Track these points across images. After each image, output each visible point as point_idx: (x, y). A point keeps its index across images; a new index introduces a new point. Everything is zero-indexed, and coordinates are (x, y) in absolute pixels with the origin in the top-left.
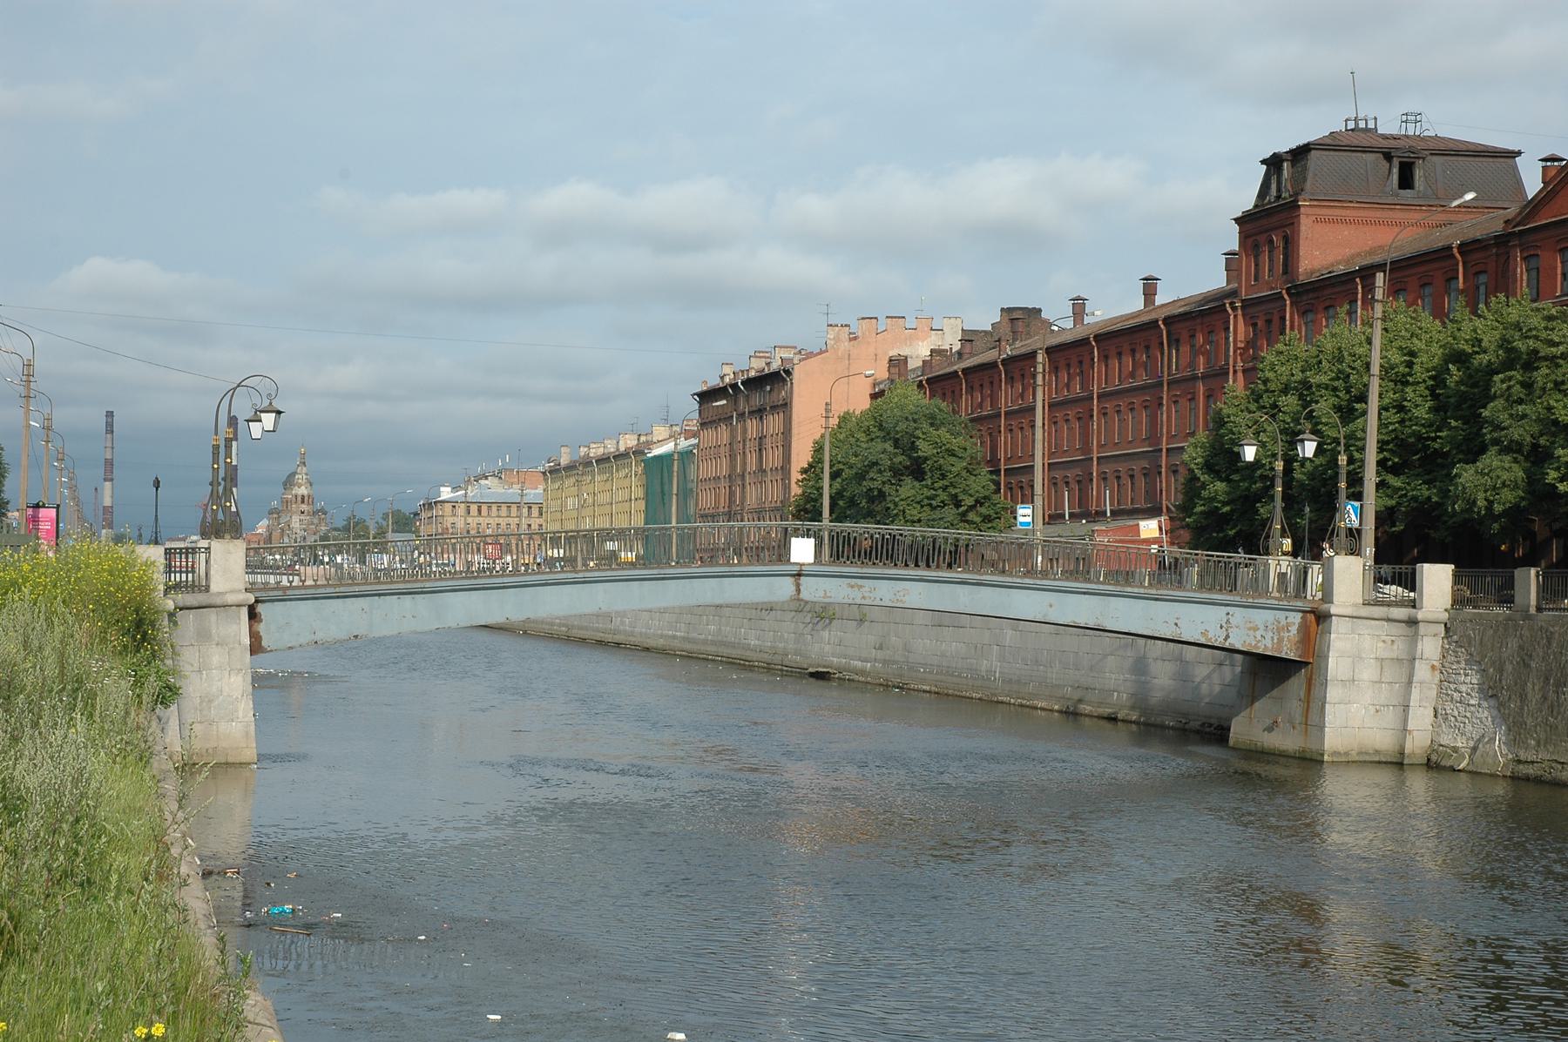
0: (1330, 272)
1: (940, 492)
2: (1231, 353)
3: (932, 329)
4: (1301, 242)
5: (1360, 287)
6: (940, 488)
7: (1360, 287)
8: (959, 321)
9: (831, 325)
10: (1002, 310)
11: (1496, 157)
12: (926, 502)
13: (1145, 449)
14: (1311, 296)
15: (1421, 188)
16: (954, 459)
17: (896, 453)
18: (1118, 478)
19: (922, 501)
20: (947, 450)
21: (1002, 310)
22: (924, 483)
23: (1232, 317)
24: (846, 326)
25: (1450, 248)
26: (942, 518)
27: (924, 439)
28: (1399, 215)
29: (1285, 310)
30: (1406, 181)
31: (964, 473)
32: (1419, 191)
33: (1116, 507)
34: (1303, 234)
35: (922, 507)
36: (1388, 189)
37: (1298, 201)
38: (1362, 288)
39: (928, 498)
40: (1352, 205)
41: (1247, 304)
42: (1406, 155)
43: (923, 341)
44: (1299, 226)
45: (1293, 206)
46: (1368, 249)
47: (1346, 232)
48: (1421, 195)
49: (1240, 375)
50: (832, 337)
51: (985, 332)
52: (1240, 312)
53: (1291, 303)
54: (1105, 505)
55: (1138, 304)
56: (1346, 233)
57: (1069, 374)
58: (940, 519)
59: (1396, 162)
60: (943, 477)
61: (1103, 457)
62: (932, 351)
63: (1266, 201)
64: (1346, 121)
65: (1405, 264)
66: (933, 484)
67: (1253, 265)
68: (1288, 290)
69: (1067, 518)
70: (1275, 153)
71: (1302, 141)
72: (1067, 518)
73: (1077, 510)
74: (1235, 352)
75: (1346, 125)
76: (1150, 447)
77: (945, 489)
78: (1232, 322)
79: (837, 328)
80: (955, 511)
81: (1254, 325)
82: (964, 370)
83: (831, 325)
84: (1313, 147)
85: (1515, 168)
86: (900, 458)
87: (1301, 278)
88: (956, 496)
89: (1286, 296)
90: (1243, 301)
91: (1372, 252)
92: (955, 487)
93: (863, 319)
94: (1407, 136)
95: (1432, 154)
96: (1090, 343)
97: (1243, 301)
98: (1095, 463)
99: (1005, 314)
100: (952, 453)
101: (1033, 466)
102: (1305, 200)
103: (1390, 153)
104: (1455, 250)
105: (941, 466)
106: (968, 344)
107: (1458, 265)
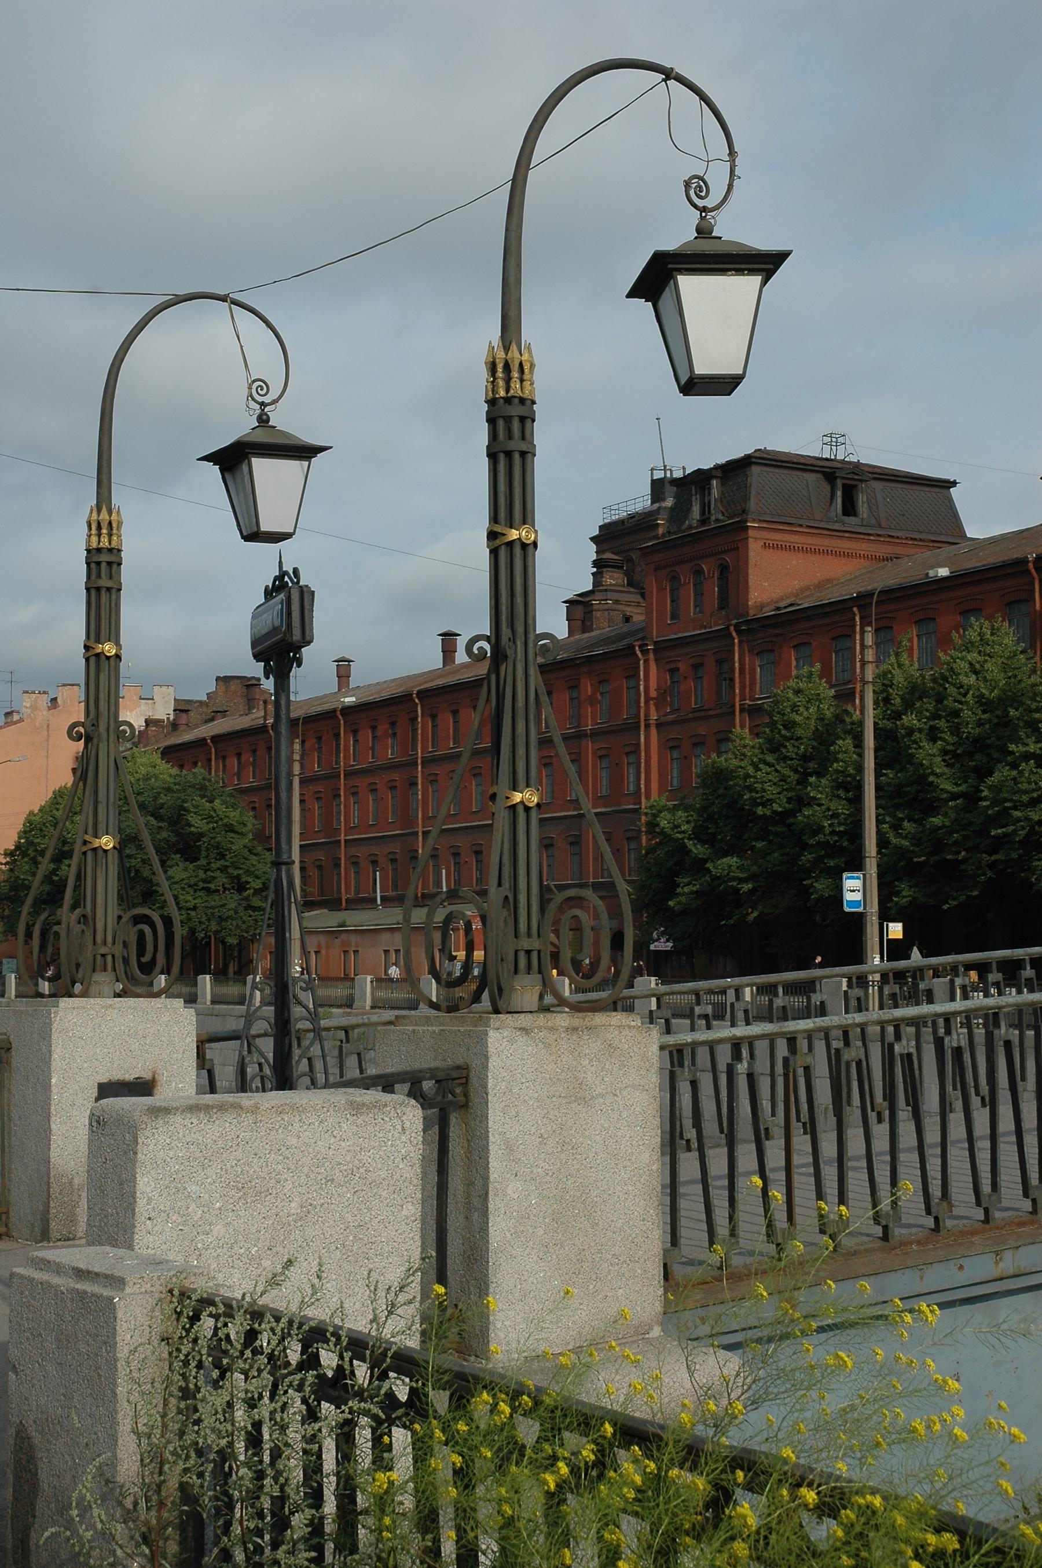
0: (791, 605)
1: (218, 874)
2: (642, 705)
3: (141, 699)
4: (750, 571)
5: (857, 619)
6: (218, 869)
7: (857, 619)
8: (171, 689)
9: (27, 692)
10: (218, 679)
11: (936, 486)
12: (201, 885)
13: (570, 813)
14: (770, 631)
15: (865, 516)
16: (233, 835)
17: (160, 827)
18: (456, 855)
19: (196, 885)
20: (225, 825)
21: (218, 679)
22: (198, 863)
23: (641, 662)
24: (44, 693)
25: (1024, 561)
26: (224, 905)
27: (195, 813)
28: (846, 545)
29: (638, 667)
30: (849, 508)
31: (246, 853)
32: (863, 519)
33: (352, 895)
34: (752, 561)
35: (195, 891)
36: (832, 515)
37: (746, 521)
38: (861, 618)
39: (204, 881)
40: (801, 530)
41: (661, 647)
42: (850, 476)
43: (131, 711)
44: (747, 552)
45: (741, 527)
46: (816, 582)
47: (795, 562)
48: (865, 523)
49: (653, 731)
50: (28, 705)
51: (200, 702)
52: (651, 656)
53: (739, 641)
54: (375, 892)
55: (435, 660)
56: (794, 562)
57: (239, 763)
58: (221, 906)
59: (839, 483)
60: (222, 856)
61: (350, 840)
62: (146, 721)
63: (684, 527)
64: (652, 470)
65: (912, 592)
66: (208, 864)
67: (669, 600)
68: (737, 627)
69: (379, 902)
70: (699, 469)
71: (738, 454)
72: (379, 902)
73: (391, 893)
74: (646, 702)
75: (652, 474)
76: (605, 807)
77: (223, 869)
78: (642, 668)
79: (34, 696)
80: (236, 896)
81: (673, 671)
82: (214, 738)
83: (27, 692)
84: (754, 460)
85: (950, 500)
86: (164, 834)
87: (751, 612)
88: (238, 877)
89: (734, 634)
90: (655, 643)
91: (820, 586)
92: (237, 868)
93: (64, 685)
94: (835, 460)
95: (875, 479)
96: (413, 700)
97: (655, 643)
98: (420, 838)
99: (220, 683)
100: (230, 829)
101: (490, 826)
102: (754, 521)
103: (834, 473)
104: (1031, 565)
105: (218, 843)
106: (184, 715)
107: (1033, 583)
